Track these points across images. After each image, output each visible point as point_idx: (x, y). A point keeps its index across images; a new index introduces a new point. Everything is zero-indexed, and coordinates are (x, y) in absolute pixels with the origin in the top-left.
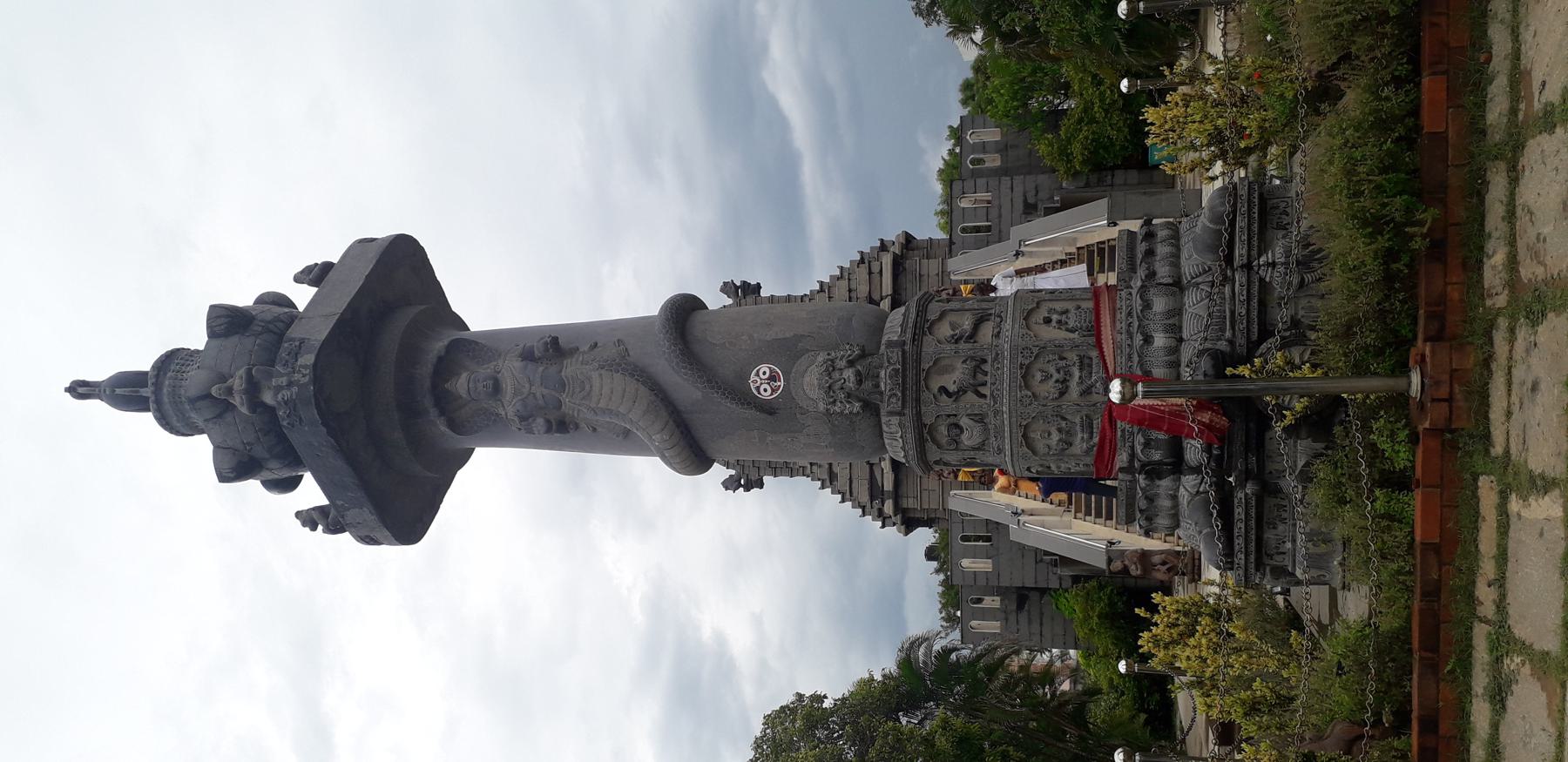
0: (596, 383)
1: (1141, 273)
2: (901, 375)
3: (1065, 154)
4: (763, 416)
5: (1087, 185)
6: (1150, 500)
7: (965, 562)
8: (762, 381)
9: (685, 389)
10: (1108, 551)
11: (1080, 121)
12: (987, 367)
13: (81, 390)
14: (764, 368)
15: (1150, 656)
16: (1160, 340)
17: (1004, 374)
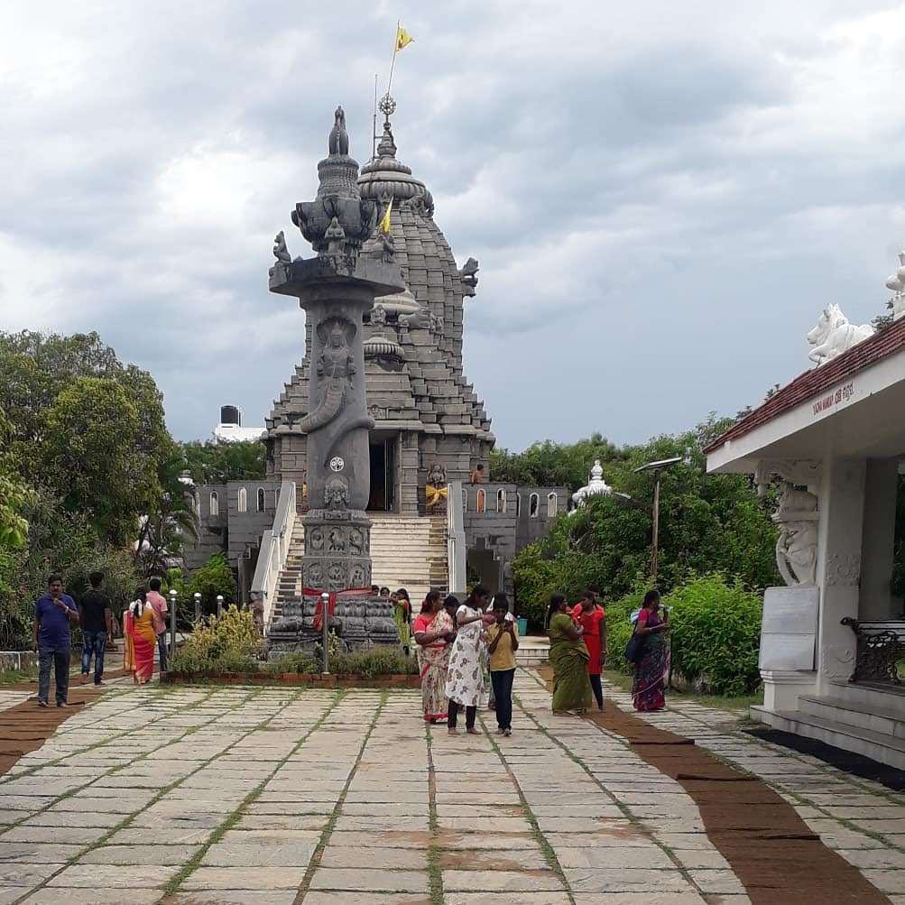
0: (336, 393)
1: (370, 604)
2: (338, 518)
3: (527, 563)
4: (324, 463)
5: (505, 579)
6: (294, 607)
7: (243, 491)
8: (338, 462)
9: (334, 430)
10: (262, 592)
11: (547, 574)
12: (341, 550)
13: (340, 116)
14: (342, 463)
15: (227, 609)
16: (347, 610)
17: (337, 556)
